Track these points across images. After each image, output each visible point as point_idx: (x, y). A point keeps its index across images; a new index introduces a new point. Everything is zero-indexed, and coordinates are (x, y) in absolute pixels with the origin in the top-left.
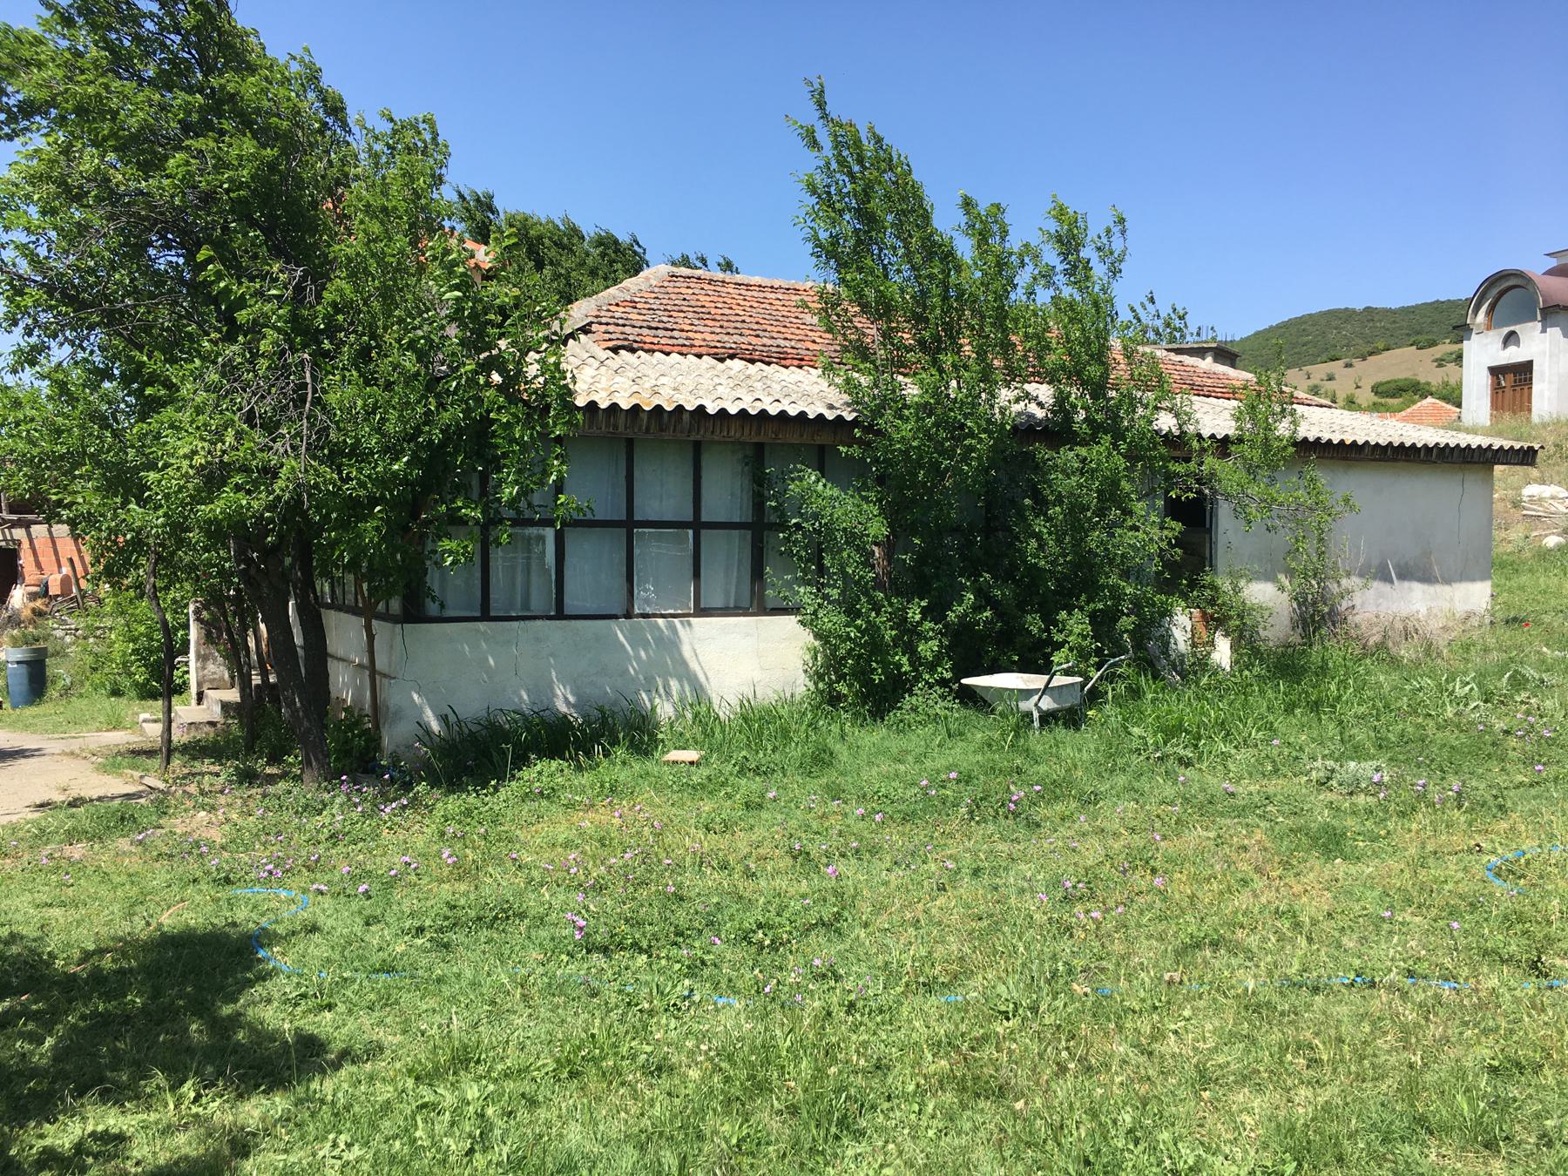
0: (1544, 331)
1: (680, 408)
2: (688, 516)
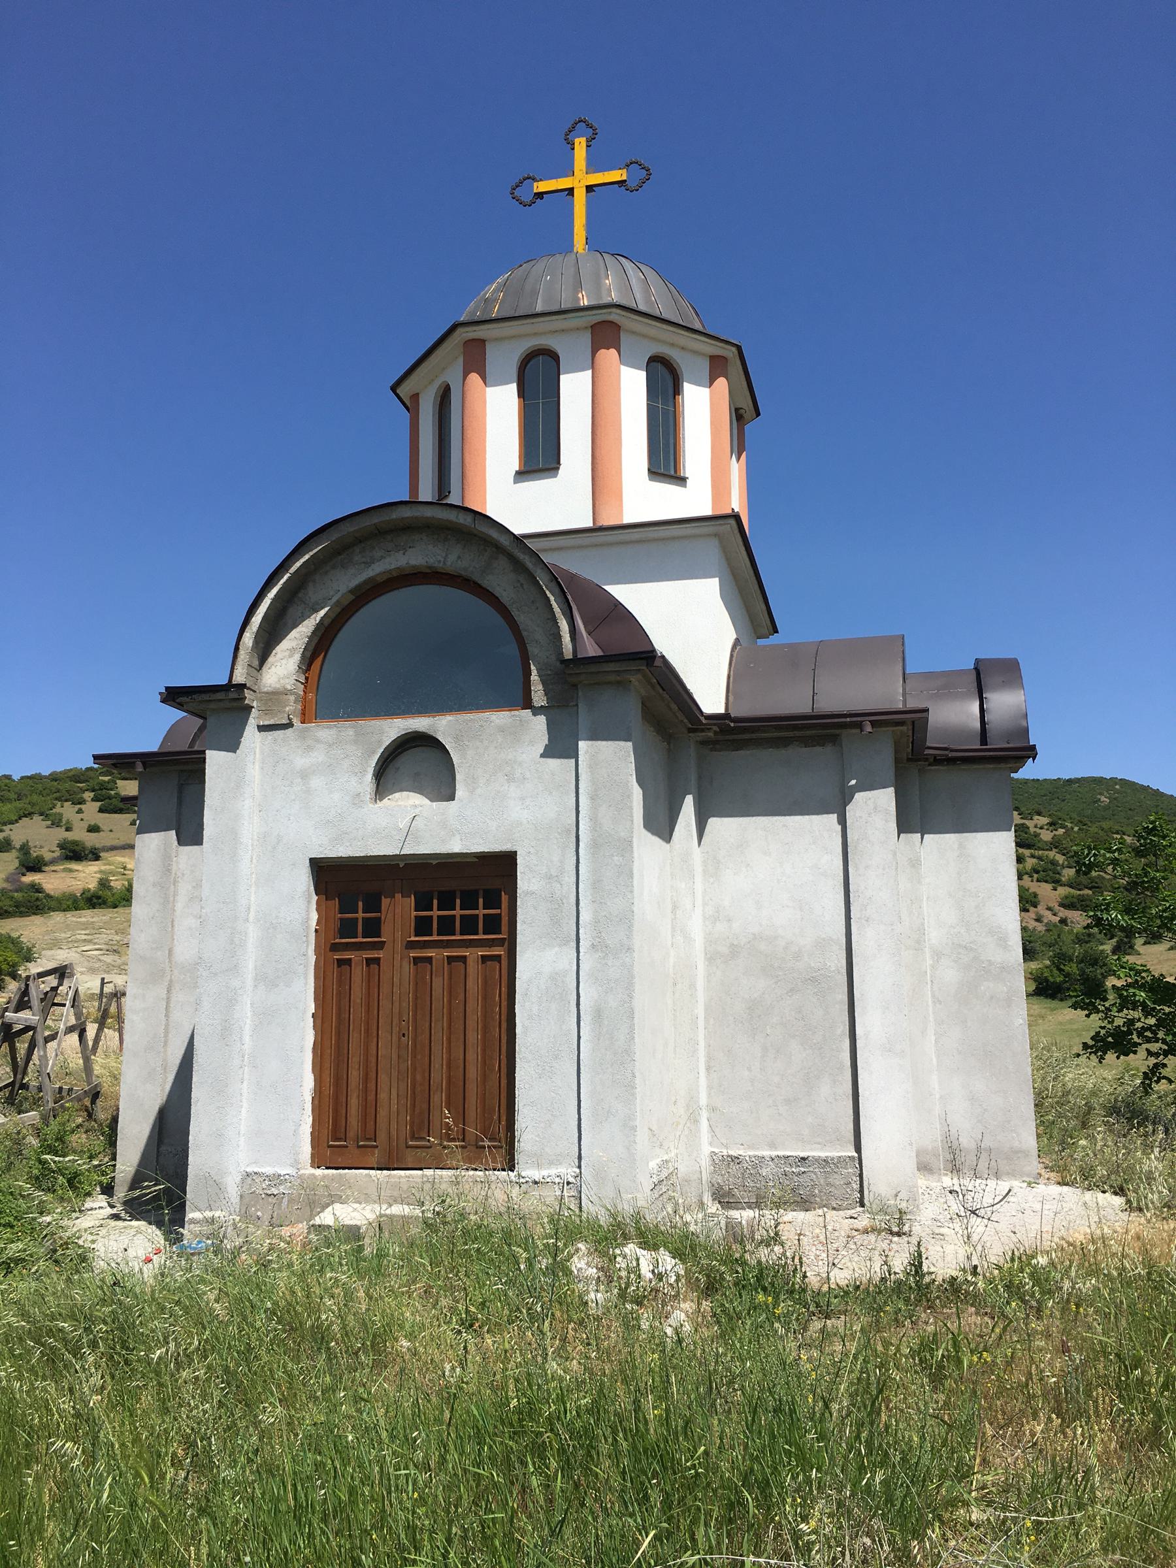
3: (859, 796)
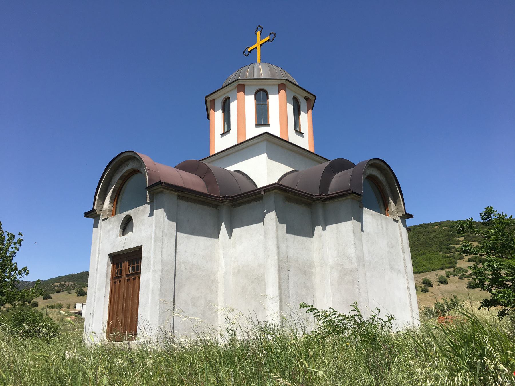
3: (267, 215)
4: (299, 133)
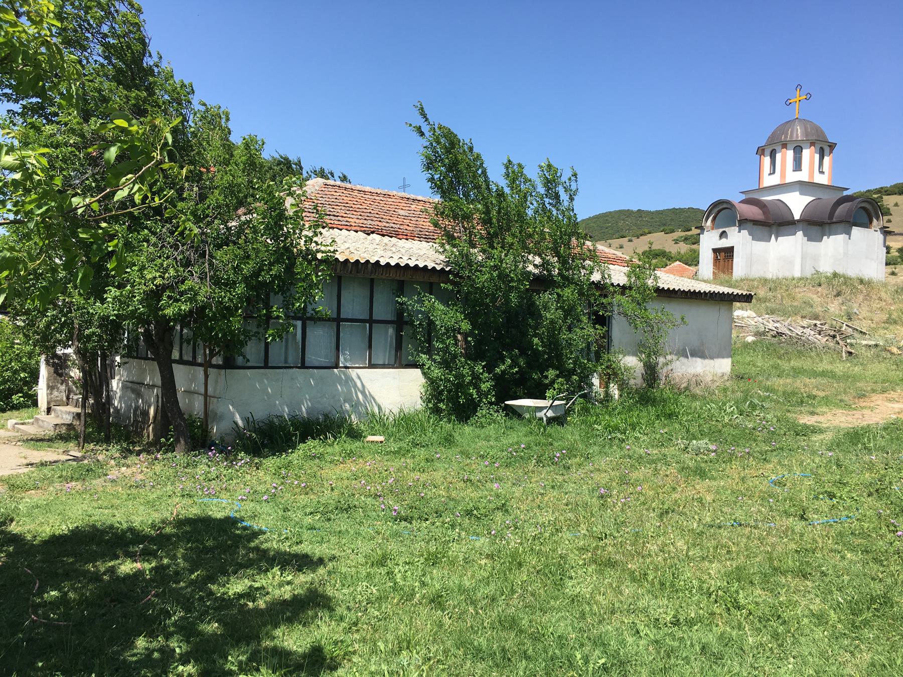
0: (739, 232)
1: (368, 261)
2: (366, 316)
4: (822, 172)
